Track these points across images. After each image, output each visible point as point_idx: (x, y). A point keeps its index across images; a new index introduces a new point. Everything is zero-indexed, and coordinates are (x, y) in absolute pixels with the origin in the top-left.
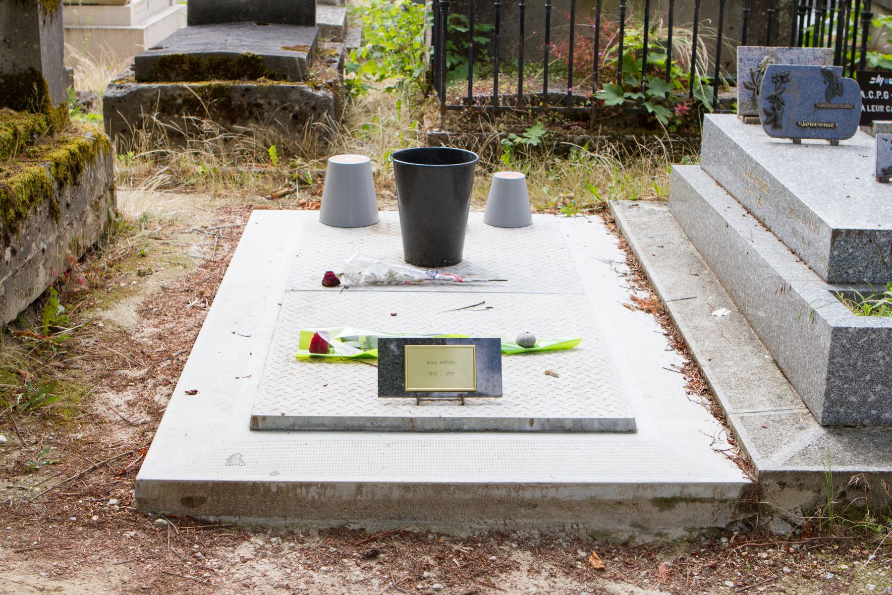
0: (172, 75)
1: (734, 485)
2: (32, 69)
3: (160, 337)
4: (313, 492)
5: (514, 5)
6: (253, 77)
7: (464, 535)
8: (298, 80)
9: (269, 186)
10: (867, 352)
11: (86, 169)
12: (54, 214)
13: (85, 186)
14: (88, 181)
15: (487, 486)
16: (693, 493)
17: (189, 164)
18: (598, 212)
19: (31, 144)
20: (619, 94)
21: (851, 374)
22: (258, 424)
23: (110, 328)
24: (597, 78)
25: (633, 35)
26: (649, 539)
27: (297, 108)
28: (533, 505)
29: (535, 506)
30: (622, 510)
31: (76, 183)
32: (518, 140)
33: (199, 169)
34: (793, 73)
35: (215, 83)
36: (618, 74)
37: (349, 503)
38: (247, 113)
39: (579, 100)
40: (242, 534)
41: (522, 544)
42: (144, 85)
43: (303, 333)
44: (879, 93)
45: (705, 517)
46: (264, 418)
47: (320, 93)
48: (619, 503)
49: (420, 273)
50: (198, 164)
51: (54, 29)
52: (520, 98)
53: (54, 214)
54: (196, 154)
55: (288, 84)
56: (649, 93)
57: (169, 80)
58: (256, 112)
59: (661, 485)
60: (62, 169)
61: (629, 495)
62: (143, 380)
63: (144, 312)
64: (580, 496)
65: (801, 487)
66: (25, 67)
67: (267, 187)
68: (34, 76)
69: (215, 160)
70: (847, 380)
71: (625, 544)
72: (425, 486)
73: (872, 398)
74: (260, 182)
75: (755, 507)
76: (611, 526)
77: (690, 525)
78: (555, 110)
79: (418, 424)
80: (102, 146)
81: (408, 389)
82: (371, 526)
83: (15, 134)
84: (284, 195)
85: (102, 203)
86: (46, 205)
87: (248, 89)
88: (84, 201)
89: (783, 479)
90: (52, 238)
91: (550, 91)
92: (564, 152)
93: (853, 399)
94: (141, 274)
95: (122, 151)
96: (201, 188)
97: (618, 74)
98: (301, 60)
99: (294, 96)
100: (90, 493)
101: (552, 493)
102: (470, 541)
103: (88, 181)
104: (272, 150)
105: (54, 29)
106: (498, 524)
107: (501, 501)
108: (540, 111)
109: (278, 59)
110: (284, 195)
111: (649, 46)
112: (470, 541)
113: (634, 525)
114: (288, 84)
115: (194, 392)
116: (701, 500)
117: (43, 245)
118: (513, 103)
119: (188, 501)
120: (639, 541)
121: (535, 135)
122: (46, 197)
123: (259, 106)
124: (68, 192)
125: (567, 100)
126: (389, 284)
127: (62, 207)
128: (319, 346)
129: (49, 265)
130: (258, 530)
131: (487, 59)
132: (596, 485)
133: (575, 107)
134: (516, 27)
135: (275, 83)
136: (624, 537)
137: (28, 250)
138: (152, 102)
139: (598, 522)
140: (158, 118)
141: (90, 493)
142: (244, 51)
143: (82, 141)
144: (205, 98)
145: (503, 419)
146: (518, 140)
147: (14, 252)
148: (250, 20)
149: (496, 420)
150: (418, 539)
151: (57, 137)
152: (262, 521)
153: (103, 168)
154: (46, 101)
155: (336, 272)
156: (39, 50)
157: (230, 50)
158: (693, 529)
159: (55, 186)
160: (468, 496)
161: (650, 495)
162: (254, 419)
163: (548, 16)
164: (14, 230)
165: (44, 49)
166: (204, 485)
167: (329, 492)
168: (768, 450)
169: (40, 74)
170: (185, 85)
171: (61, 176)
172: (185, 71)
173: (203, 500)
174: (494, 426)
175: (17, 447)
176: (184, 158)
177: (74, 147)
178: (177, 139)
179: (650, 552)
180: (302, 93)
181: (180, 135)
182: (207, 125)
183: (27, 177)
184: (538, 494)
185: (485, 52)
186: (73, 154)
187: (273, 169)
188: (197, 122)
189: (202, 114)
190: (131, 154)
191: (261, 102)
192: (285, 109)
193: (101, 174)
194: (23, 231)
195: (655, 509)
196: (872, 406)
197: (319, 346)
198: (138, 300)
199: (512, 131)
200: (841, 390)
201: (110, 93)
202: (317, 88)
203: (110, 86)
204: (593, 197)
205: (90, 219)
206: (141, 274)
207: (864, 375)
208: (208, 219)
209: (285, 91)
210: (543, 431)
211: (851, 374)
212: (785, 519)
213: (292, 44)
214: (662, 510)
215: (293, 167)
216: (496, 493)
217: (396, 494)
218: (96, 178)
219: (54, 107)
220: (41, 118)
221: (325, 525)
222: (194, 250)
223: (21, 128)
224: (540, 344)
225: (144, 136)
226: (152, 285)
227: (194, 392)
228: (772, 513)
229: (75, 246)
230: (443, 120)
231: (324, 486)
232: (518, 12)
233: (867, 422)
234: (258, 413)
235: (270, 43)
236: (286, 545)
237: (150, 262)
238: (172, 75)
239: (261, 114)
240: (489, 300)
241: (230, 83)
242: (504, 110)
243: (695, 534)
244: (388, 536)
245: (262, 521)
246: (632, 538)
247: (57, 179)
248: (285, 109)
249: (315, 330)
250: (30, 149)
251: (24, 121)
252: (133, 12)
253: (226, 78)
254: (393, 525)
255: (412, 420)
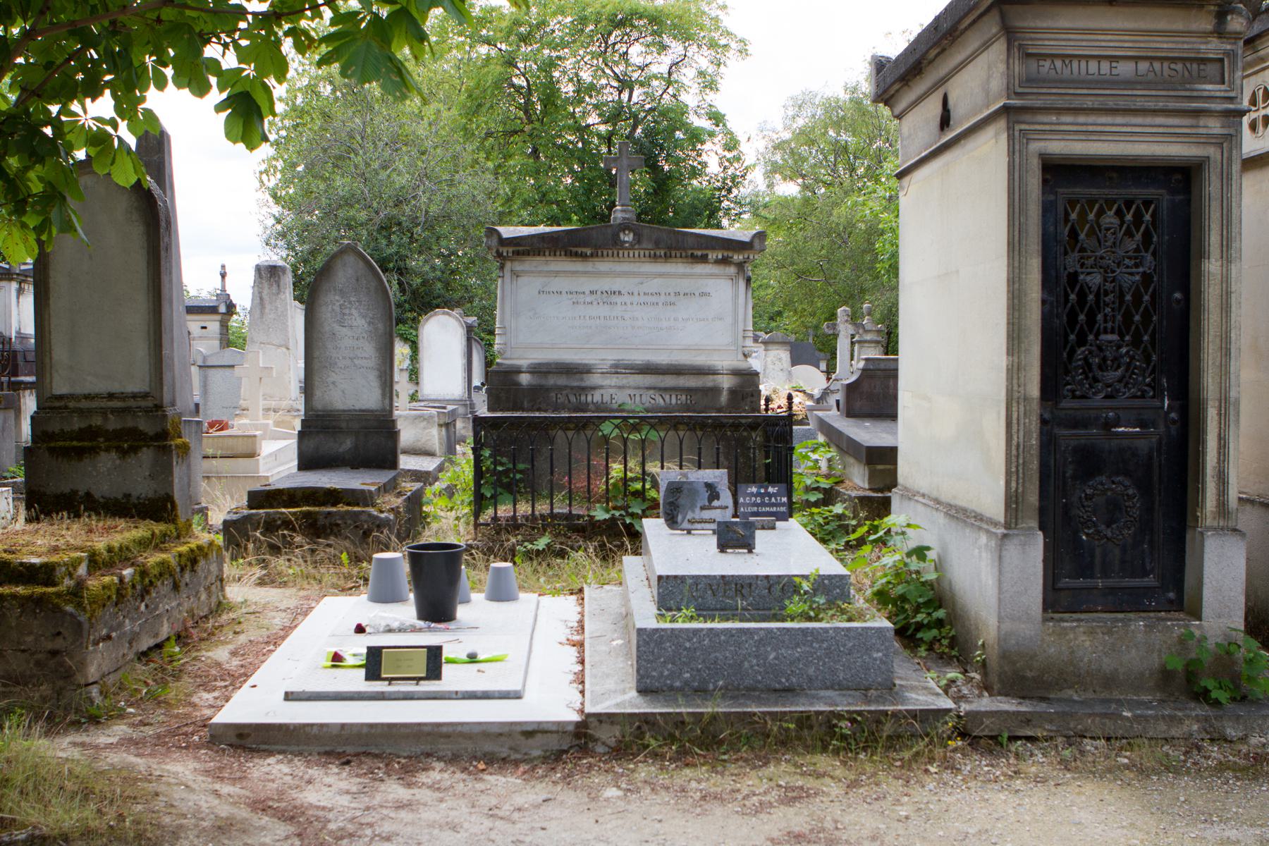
0: (275, 504)
1: (569, 723)
2: (167, 494)
3: (242, 666)
4: (315, 730)
5: (544, 450)
6: (334, 505)
7: (405, 754)
8: (368, 506)
9: (341, 582)
10: (659, 643)
11: (202, 563)
12: (176, 587)
13: (201, 574)
14: (203, 570)
15: (419, 724)
16: (546, 727)
17: (283, 568)
18: (576, 593)
19: (164, 543)
20: (607, 511)
21: (651, 658)
22: (289, 697)
23: (209, 661)
24: (589, 497)
25: (616, 469)
26: (518, 756)
27: (366, 526)
28: (447, 736)
29: (449, 737)
30: (502, 739)
31: (193, 570)
32: (530, 546)
33: (291, 571)
34: (685, 486)
35: (305, 509)
36: (606, 497)
37: (337, 736)
38: (329, 531)
39: (579, 517)
40: (271, 753)
41: (439, 759)
42: (253, 511)
43: (329, 652)
44: (753, 499)
45: (554, 743)
46: (292, 693)
47: (383, 516)
48: (501, 734)
49: (421, 624)
50: (290, 567)
51: (184, 468)
52: (532, 518)
53: (176, 587)
54: (289, 560)
55: (359, 509)
56: (630, 510)
57: (272, 507)
58: (335, 530)
59: (526, 723)
60: (184, 560)
61: (506, 729)
62: (226, 687)
63: (234, 654)
64: (477, 730)
65: (612, 723)
66: (162, 493)
67: (339, 583)
68: (169, 498)
69: (303, 564)
70: (648, 661)
71: (504, 759)
72: (383, 725)
73: (666, 673)
74: (335, 580)
75: (585, 735)
76: (496, 749)
77: (545, 748)
78: (559, 525)
79: (386, 695)
80: (215, 548)
81: (384, 676)
82: (350, 749)
83: (153, 534)
84: (351, 589)
85: (213, 588)
86: (171, 580)
87: (329, 513)
88: (200, 584)
89: (602, 718)
90: (174, 604)
91: (556, 511)
92: (562, 554)
93: (654, 674)
94: (235, 633)
95: (234, 558)
96: (291, 584)
97: (606, 497)
98: (370, 492)
99: (363, 518)
100: (183, 734)
101: (459, 728)
102: (410, 757)
103: (203, 570)
104: (344, 556)
105: (184, 468)
106: (428, 748)
107: (429, 734)
108: (548, 525)
109: (353, 491)
110: (351, 589)
111: (629, 475)
112: (410, 757)
113: (511, 748)
114: (359, 509)
115: (255, 686)
116: (551, 732)
117: (167, 607)
118: (527, 520)
119: (240, 736)
120: (512, 757)
121: (542, 543)
122: (171, 575)
123: (338, 525)
124: (187, 576)
125: (569, 516)
126: (400, 631)
127: (182, 584)
128: (337, 658)
129: (172, 620)
130: (280, 753)
131: (523, 490)
132: (485, 723)
133: (576, 522)
134: (547, 466)
135: (350, 508)
136: (504, 755)
137: (156, 608)
138: (259, 524)
139: (488, 747)
140: (261, 533)
141: (183, 734)
142: (328, 486)
143: (200, 543)
144: (296, 519)
145: (438, 692)
146: (530, 546)
147: (147, 606)
148: (346, 466)
149: (434, 692)
150: (376, 756)
151: (182, 540)
152: (284, 748)
153: (215, 564)
154: (176, 515)
155: (364, 625)
156: (172, 481)
157: (319, 485)
158: (547, 751)
159: (178, 570)
160: (408, 731)
161: (519, 729)
162: (287, 694)
163: (552, 455)
164: (148, 592)
165: (176, 481)
166: (250, 726)
167: (325, 729)
168: (594, 703)
169: (173, 497)
170: (283, 510)
171: (182, 563)
172: (284, 501)
173: (249, 735)
174: (434, 695)
175: (140, 715)
176: (280, 563)
177: (193, 546)
178: (275, 550)
179: (516, 763)
180: (370, 515)
181: (279, 548)
182: (298, 539)
183: (158, 560)
184: (451, 729)
185: (522, 485)
186: (192, 550)
187: (346, 571)
188: (290, 536)
189: (294, 530)
190: (241, 561)
191: (339, 522)
192: (357, 527)
193: (214, 568)
194: (154, 595)
195: (523, 738)
196: (667, 677)
197: (337, 658)
198: (231, 647)
199: (528, 541)
200: (647, 669)
201: (228, 518)
202: (382, 512)
203: (229, 512)
204: (576, 587)
205: (203, 597)
206: (235, 633)
207: (660, 658)
208: (292, 603)
209: (357, 514)
210: (464, 698)
211: (651, 658)
212: (604, 743)
213: (369, 481)
214: (527, 739)
215: (361, 568)
216: (426, 729)
217: (365, 730)
218: (209, 570)
219: (181, 520)
220: (172, 527)
221: (322, 749)
222: (277, 621)
223: (157, 532)
224: (480, 657)
225: (251, 546)
226: (242, 639)
227: (255, 686)
228: (596, 740)
229: (191, 612)
230: (476, 534)
231: (322, 725)
232: (548, 454)
233: (665, 688)
234: (289, 690)
235: (353, 481)
236: (296, 759)
237: (244, 626)
238: (275, 504)
239: (339, 531)
240: (461, 638)
241: (317, 509)
242: (522, 525)
243: (548, 754)
244: (357, 755)
245: (284, 748)
246: (509, 756)
247: (180, 565)
248: (357, 527)
249: (334, 650)
250: (162, 546)
251: (159, 528)
252: (261, 462)
253: (315, 505)
254: (363, 749)
255: (383, 693)
